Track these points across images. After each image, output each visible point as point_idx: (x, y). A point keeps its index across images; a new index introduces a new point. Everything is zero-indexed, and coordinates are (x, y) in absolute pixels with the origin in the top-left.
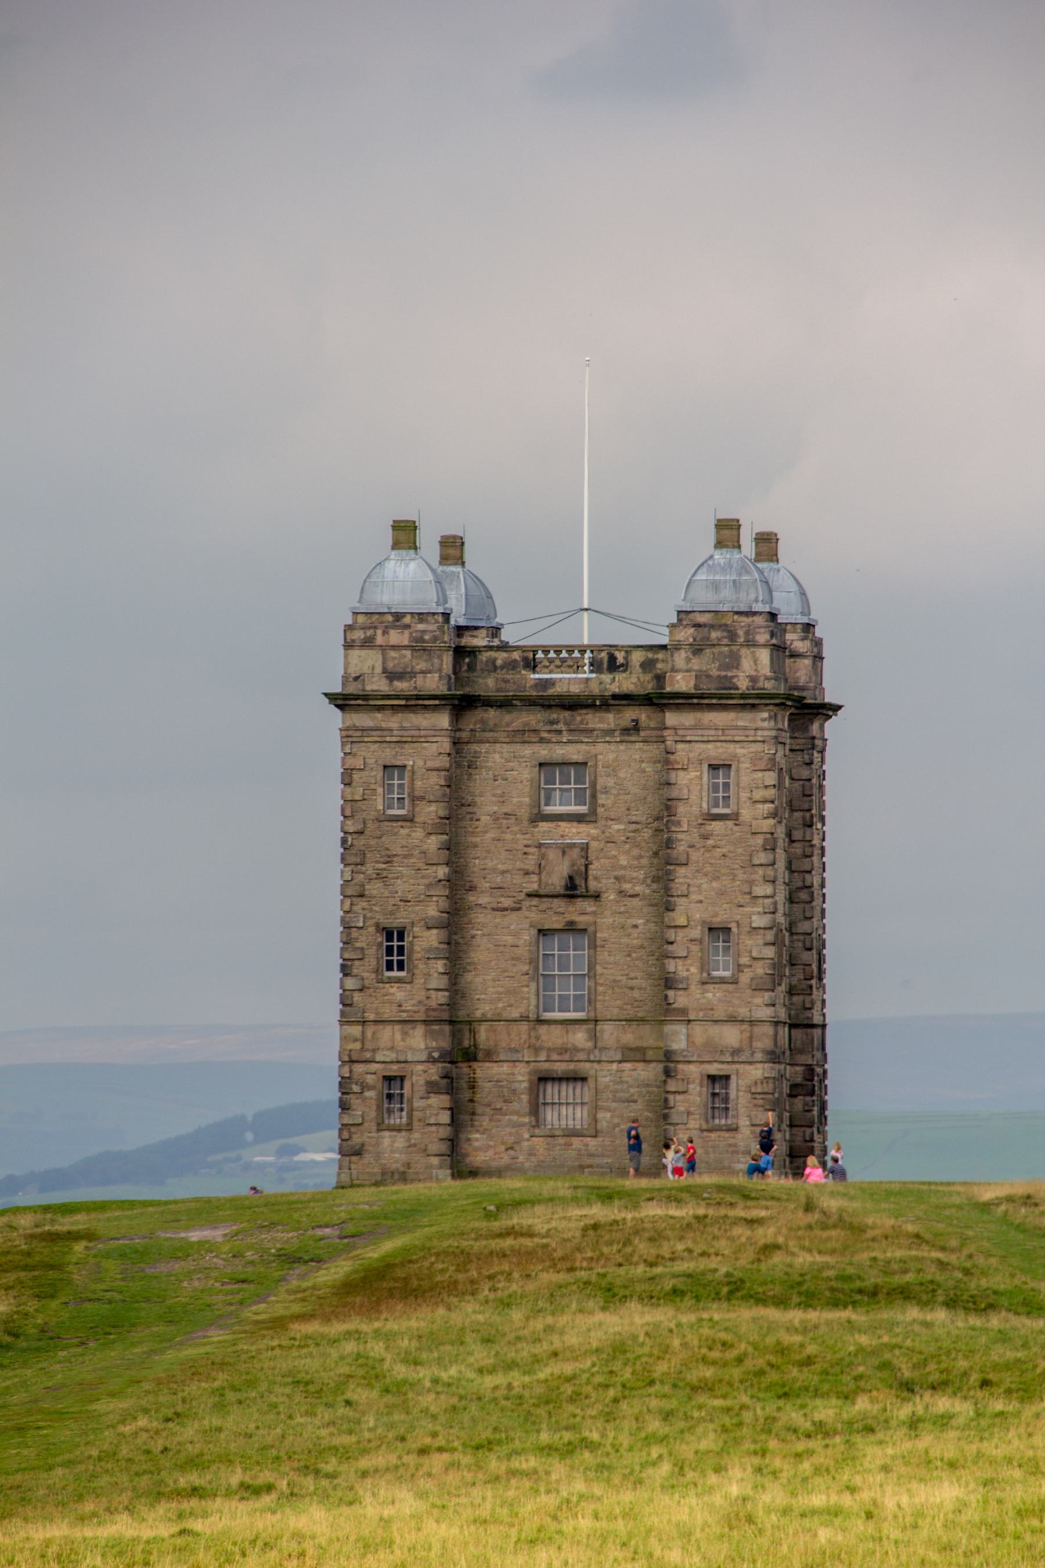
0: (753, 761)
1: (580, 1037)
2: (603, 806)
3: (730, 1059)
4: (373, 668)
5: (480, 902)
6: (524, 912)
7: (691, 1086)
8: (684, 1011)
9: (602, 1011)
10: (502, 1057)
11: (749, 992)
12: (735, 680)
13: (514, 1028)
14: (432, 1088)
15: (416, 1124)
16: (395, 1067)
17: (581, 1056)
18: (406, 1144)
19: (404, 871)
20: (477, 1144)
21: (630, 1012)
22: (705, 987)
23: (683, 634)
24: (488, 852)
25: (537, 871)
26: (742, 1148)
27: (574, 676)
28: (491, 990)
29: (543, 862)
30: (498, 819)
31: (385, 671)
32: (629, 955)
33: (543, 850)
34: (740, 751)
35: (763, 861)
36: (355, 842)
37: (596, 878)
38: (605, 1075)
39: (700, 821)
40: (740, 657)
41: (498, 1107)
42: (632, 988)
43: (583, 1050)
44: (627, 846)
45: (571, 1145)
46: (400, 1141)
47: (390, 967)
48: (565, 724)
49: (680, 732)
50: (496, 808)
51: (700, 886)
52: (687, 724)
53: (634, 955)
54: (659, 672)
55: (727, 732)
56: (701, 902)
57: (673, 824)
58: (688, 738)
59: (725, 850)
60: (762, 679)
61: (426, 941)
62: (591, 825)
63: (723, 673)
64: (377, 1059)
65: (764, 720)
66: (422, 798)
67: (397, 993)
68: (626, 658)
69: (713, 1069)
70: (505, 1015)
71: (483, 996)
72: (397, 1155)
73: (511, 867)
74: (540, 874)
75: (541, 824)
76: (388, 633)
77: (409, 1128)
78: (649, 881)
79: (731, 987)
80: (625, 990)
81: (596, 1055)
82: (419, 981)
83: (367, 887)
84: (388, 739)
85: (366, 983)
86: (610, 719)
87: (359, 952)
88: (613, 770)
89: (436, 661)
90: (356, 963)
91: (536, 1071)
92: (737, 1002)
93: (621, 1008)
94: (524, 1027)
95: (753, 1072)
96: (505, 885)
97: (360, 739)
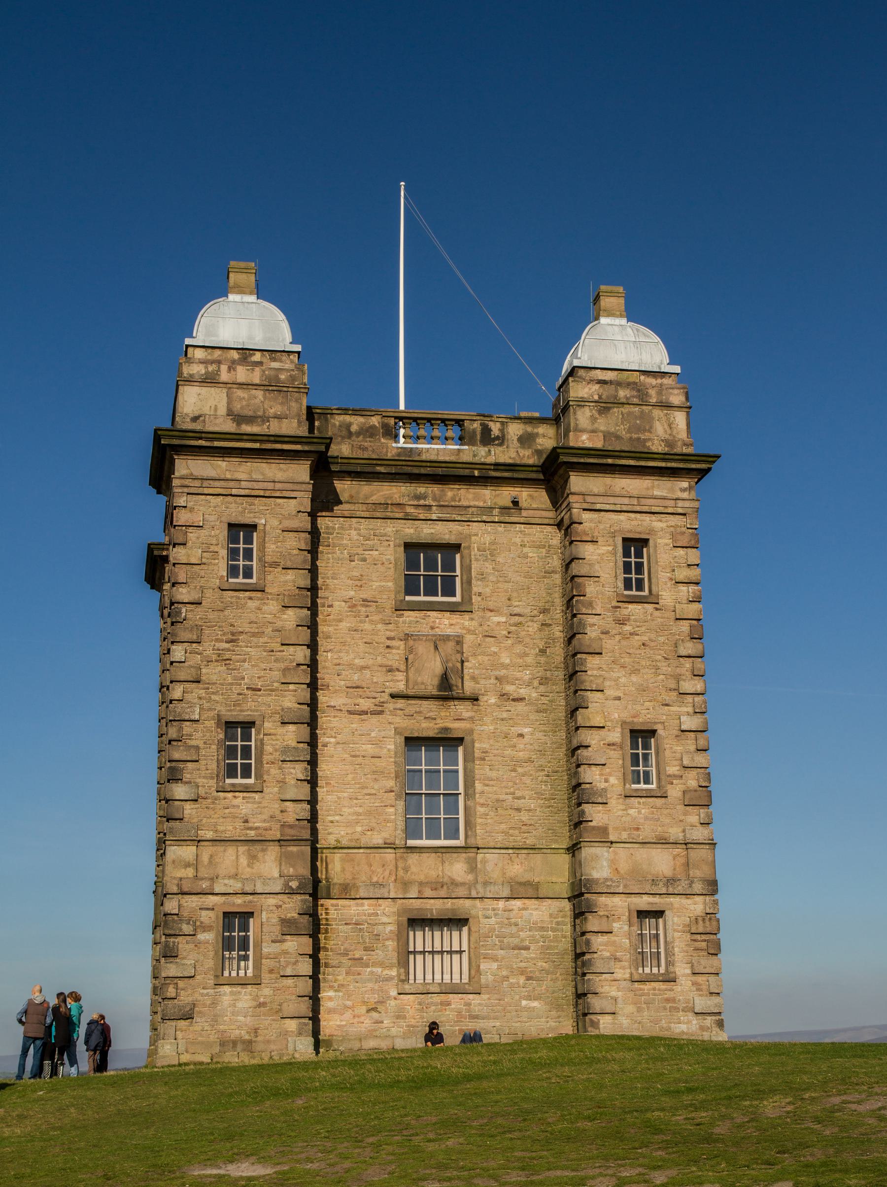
0: (673, 536)
1: (457, 869)
2: (480, 594)
3: (664, 891)
4: (216, 409)
5: (332, 704)
6: (387, 717)
7: (616, 925)
8: (604, 830)
9: (481, 836)
10: (362, 894)
11: (681, 807)
12: (649, 444)
13: (376, 856)
14: (288, 928)
15: (266, 977)
16: (239, 900)
17: (462, 891)
18: (255, 1003)
19: (253, 651)
20: (330, 1004)
21: (519, 839)
22: (628, 800)
23: (586, 390)
24: (344, 643)
25: (403, 668)
26: (682, 1006)
27: (444, 446)
28: (346, 810)
29: (411, 657)
30: (355, 606)
31: (230, 413)
32: (514, 770)
33: (411, 643)
34: (657, 523)
35: (690, 652)
36: (190, 615)
37: (473, 678)
38: (487, 915)
39: (615, 604)
40: (653, 418)
41: (357, 956)
42: (519, 810)
43: (463, 884)
44: (510, 642)
45: (449, 1004)
46: (245, 998)
47: (231, 772)
48: (434, 500)
49: (589, 499)
50: (352, 593)
51: (616, 680)
52: (596, 491)
53: (520, 770)
54: (539, 447)
55: (643, 501)
56: (619, 699)
57: (584, 606)
58: (598, 507)
59: (645, 638)
60: (679, 443)
61: (279, 738)
62: (467, 616)
63: (635, 436)
64: (217, 890)
65: (683, 490)
66: (275, 565)
67: (243, 805)
68: (502, 430)
69: (644, 902)
70: (364, 841)
71: (337, 818)
72: (241, 1018)
73: (371, 662)
74: (407, 671)
75: (406, 613)
76: (235, 370)
77: (256, 982)
78: (536, 683)
79: (659, 802)
80: (510, 812)
81: (481, 890)
82: (271, 790)
83: (204, 671)
84: (234, 492)
85: (202, 791)
86: (487, 495)
87: (193, 751)
88: (490, 553)
89: (293, 404)
90: (189, 765)
91: (406, 910)
92: (668, 821)
93: (505, 833)
94: (389, 856)
95: (692, 907)
96: (364, 685)
97: (200, 491)
